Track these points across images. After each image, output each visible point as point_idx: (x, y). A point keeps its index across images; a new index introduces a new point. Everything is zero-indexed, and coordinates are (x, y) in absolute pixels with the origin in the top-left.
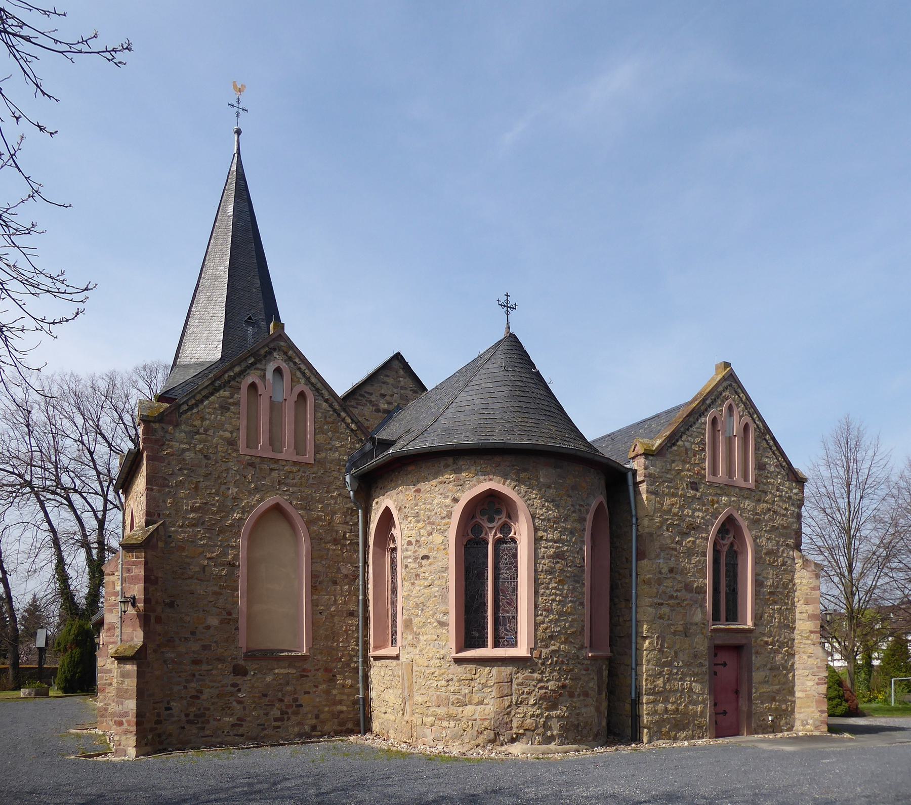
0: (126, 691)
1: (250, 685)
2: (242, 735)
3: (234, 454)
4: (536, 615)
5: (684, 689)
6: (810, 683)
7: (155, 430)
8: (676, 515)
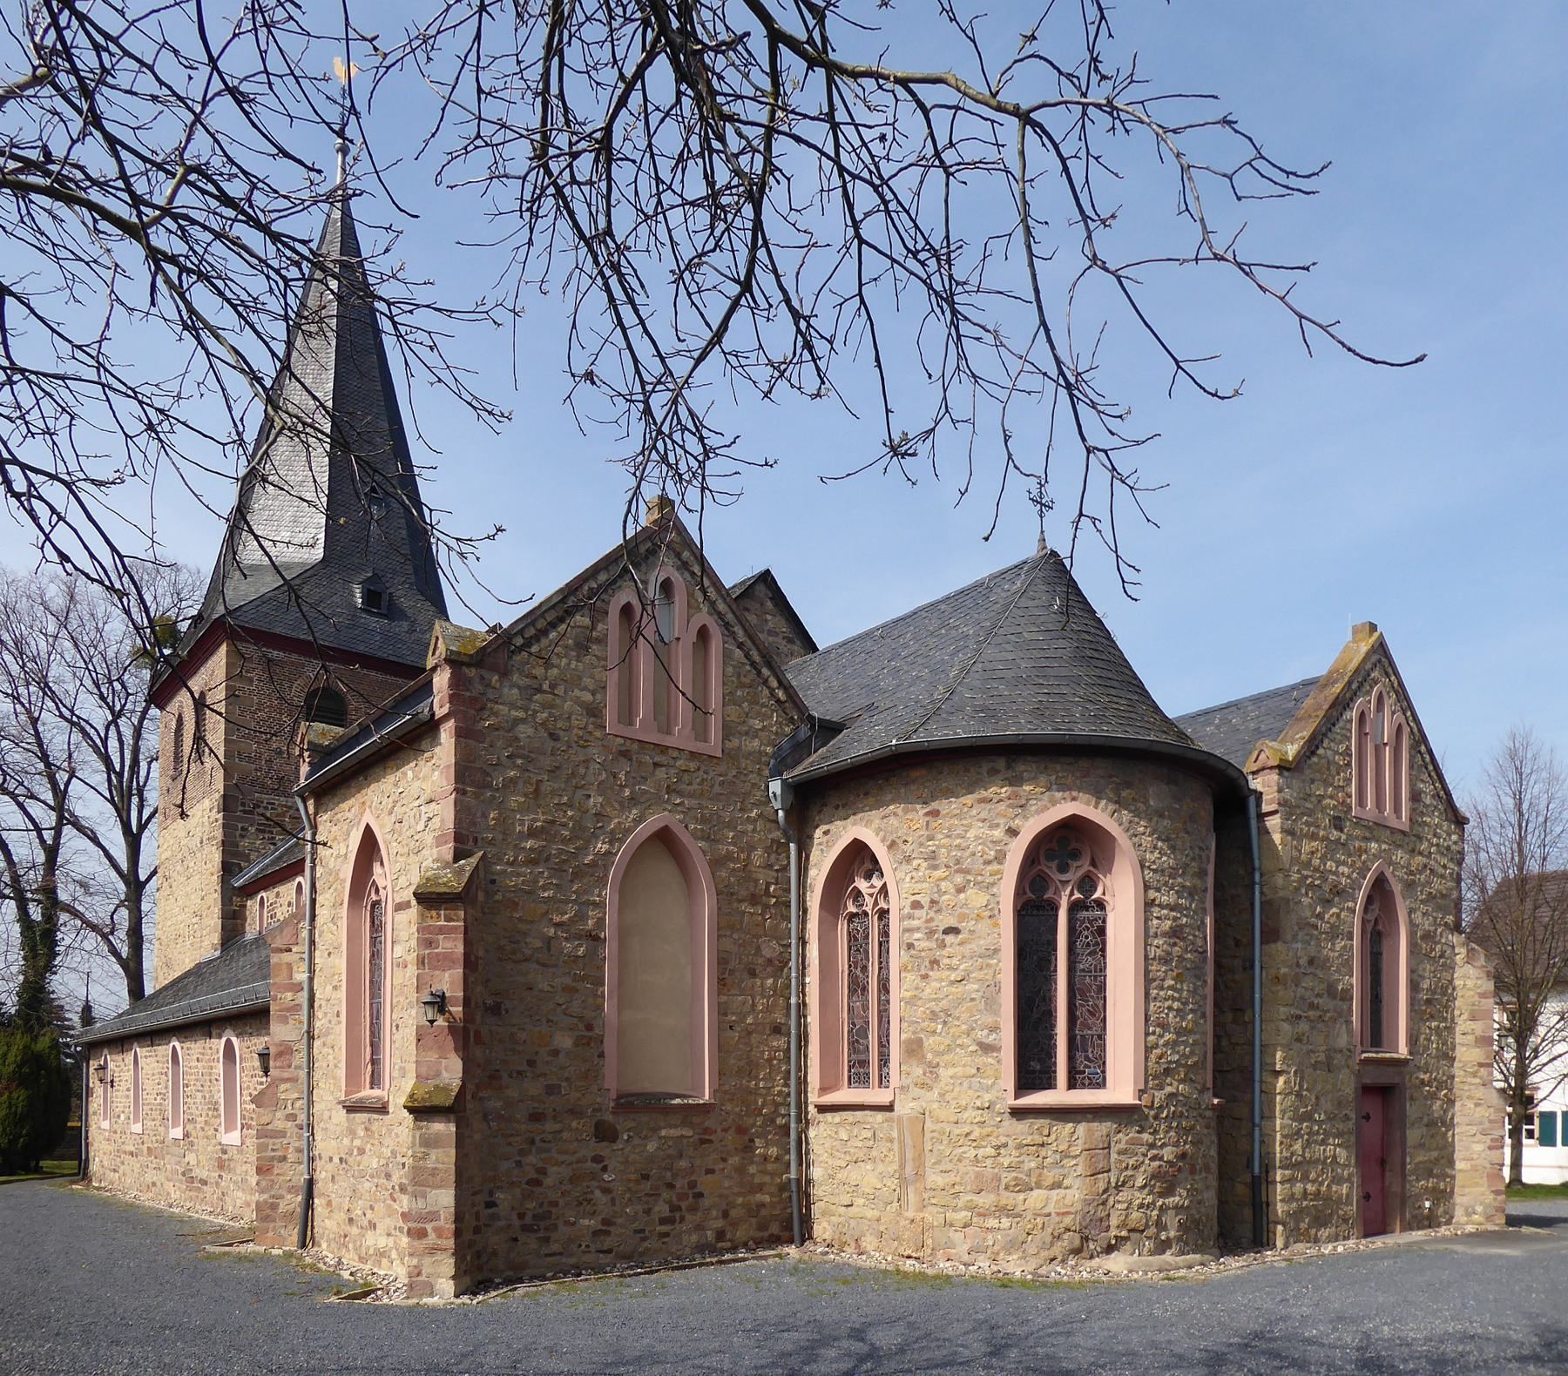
0: (434, 1172)
1: (621, 1159)
2: (609, 1251)
3: (598, 734)
4: (1147, 1034)
5: (1326, 1158)
6: (1478, 1148)
7: (470, 680)
8: (1316, 870)
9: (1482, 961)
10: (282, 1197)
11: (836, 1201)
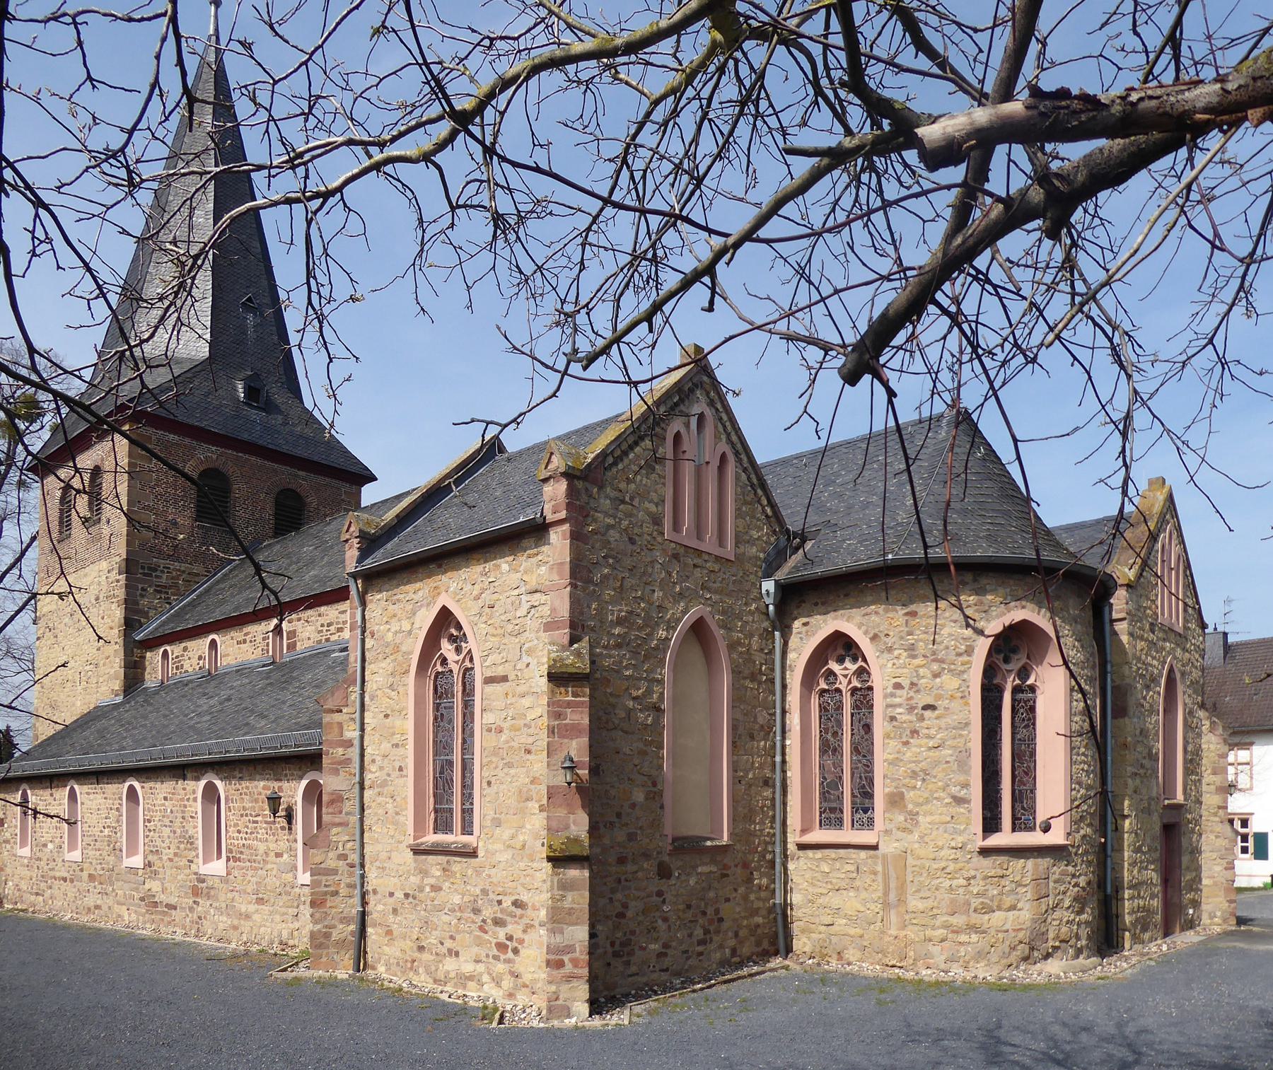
0: (570, 912)
2: (667, 970)
3: (659, 539)
6: (1218, 868)
9: (1220, 731)
10: (334, 927)
11: (817, 921)
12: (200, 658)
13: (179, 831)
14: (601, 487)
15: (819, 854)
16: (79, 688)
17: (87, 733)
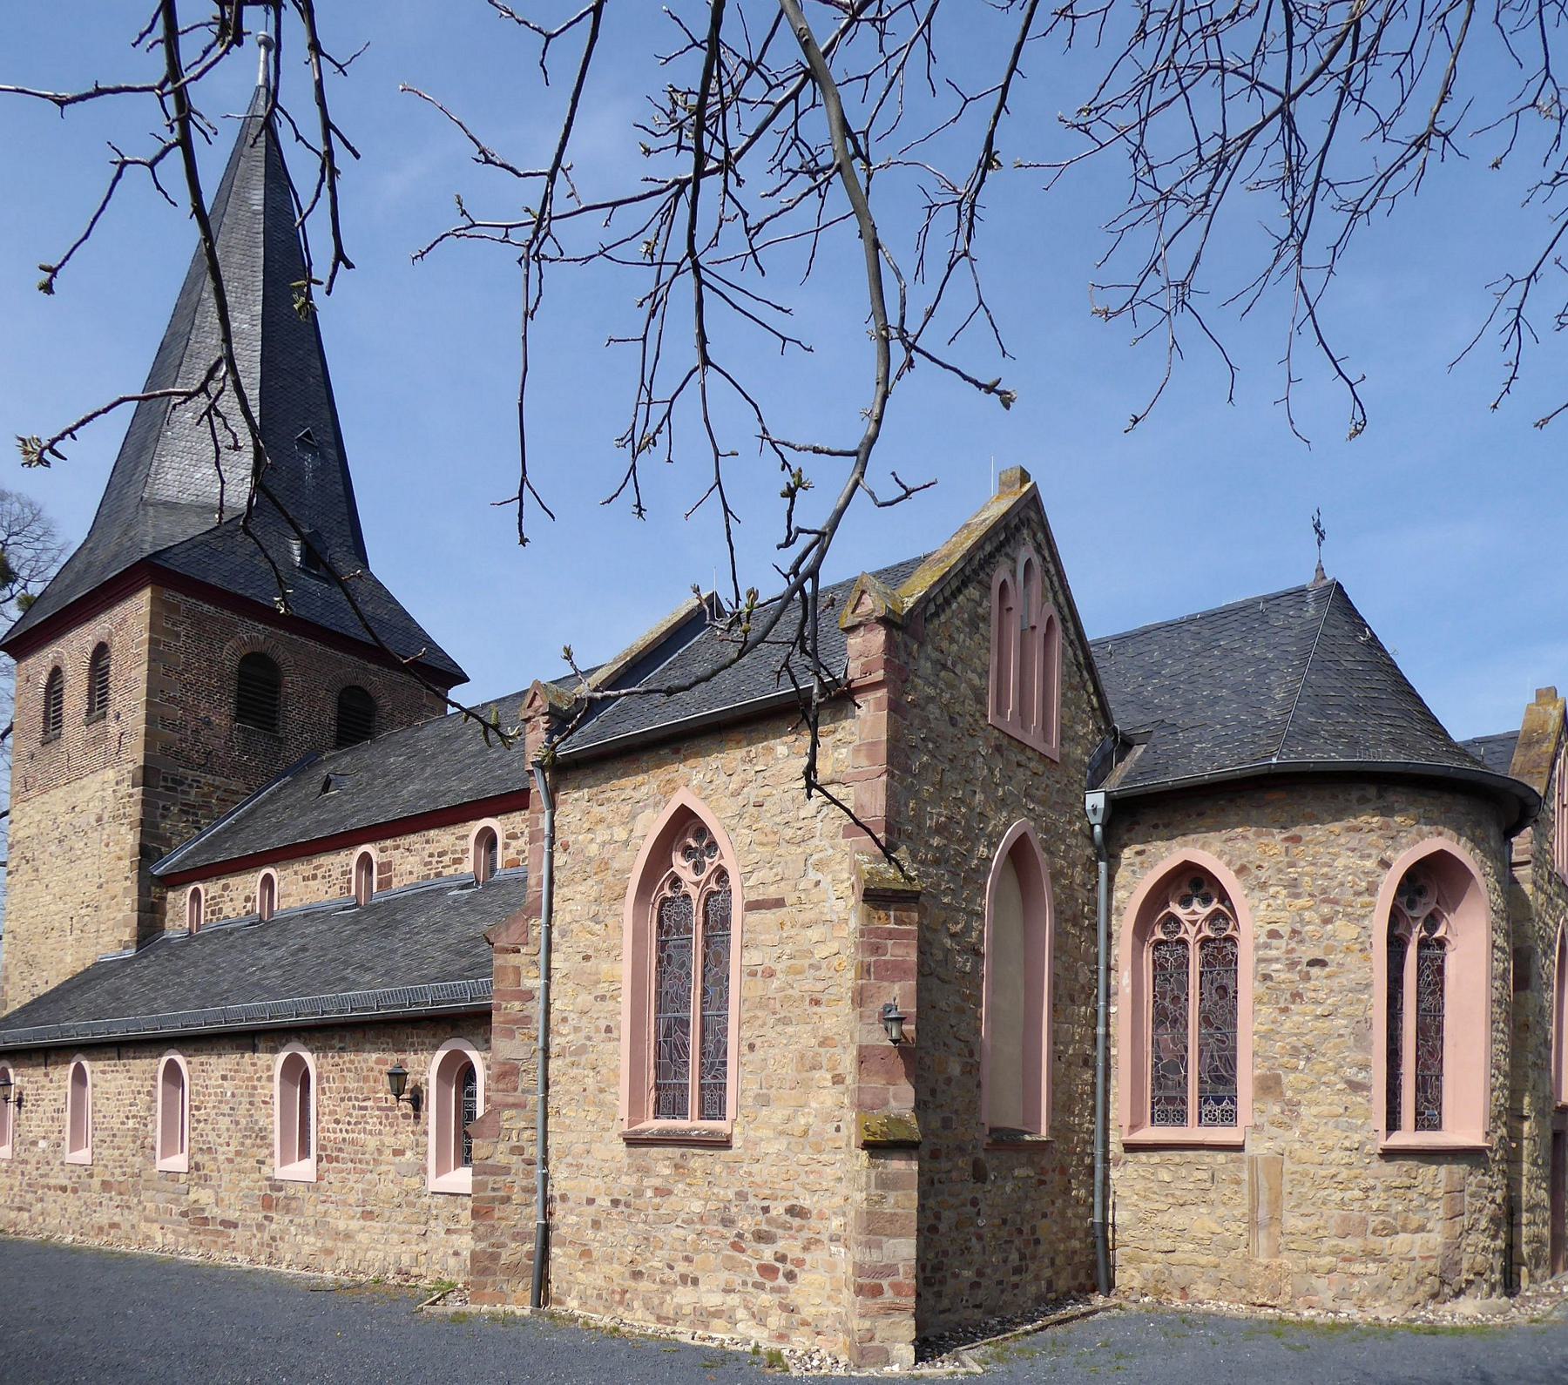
0: (892, 1219)
10: (503, 1245)
11: (1151, 1246)
12: (247, 899)
13: (243, 1122)
14: (921, 644)
15: (1156, 1157)
16: (70, 938)
17: (91, 995)
